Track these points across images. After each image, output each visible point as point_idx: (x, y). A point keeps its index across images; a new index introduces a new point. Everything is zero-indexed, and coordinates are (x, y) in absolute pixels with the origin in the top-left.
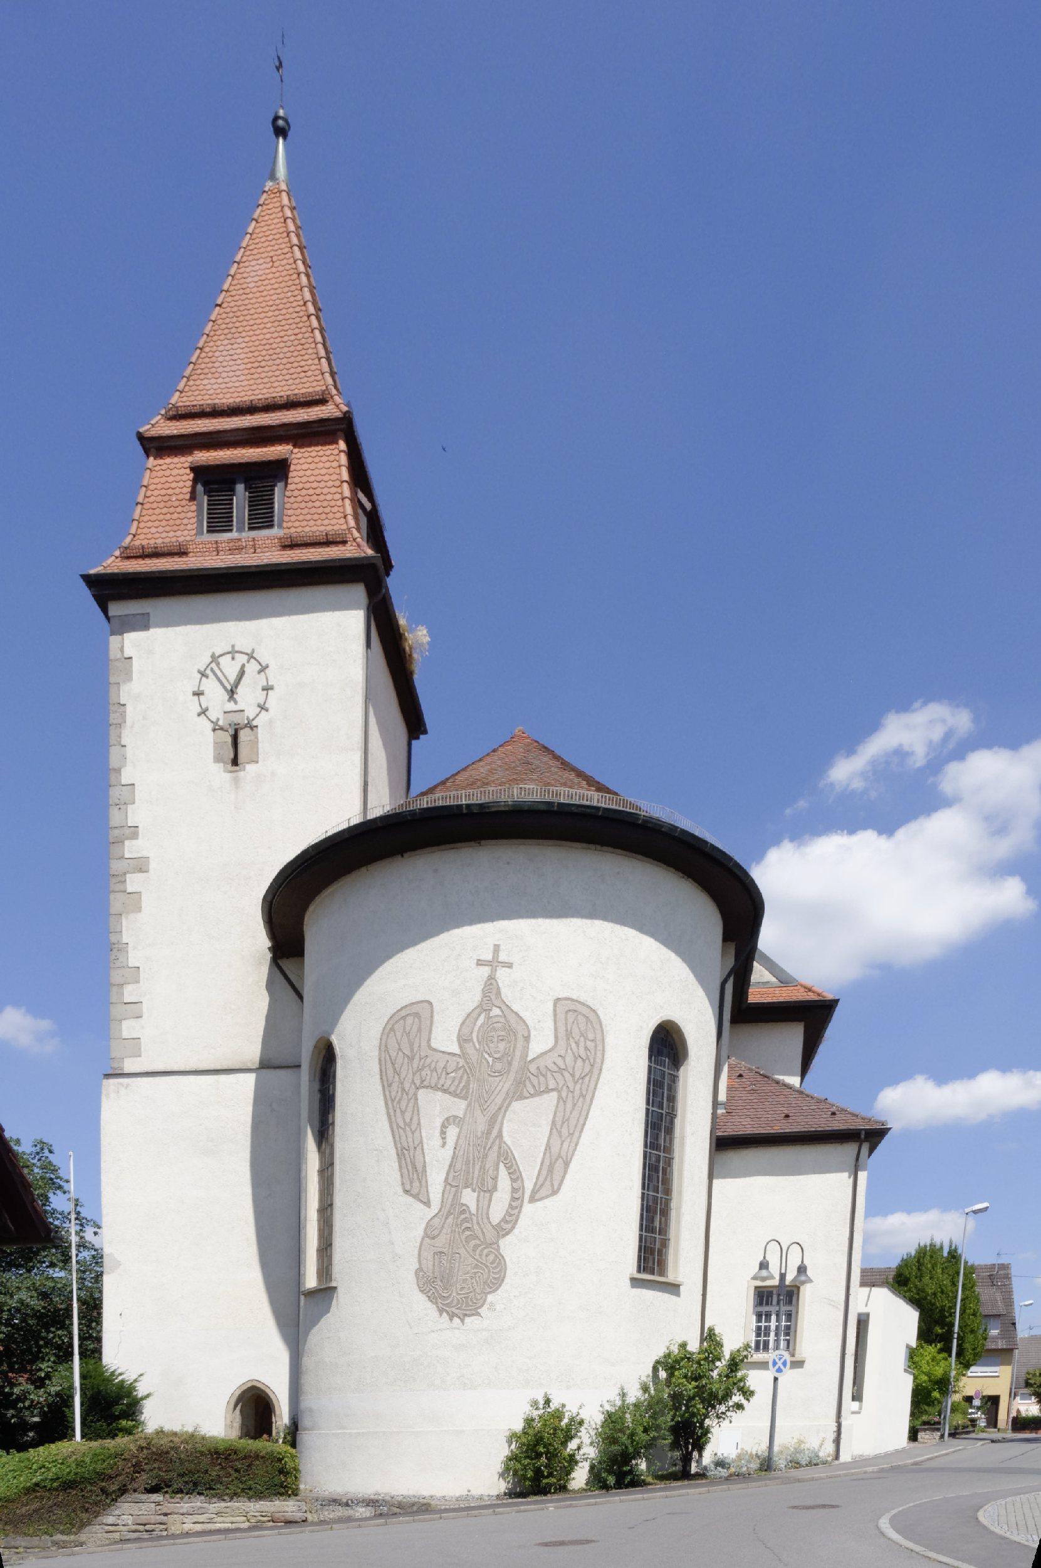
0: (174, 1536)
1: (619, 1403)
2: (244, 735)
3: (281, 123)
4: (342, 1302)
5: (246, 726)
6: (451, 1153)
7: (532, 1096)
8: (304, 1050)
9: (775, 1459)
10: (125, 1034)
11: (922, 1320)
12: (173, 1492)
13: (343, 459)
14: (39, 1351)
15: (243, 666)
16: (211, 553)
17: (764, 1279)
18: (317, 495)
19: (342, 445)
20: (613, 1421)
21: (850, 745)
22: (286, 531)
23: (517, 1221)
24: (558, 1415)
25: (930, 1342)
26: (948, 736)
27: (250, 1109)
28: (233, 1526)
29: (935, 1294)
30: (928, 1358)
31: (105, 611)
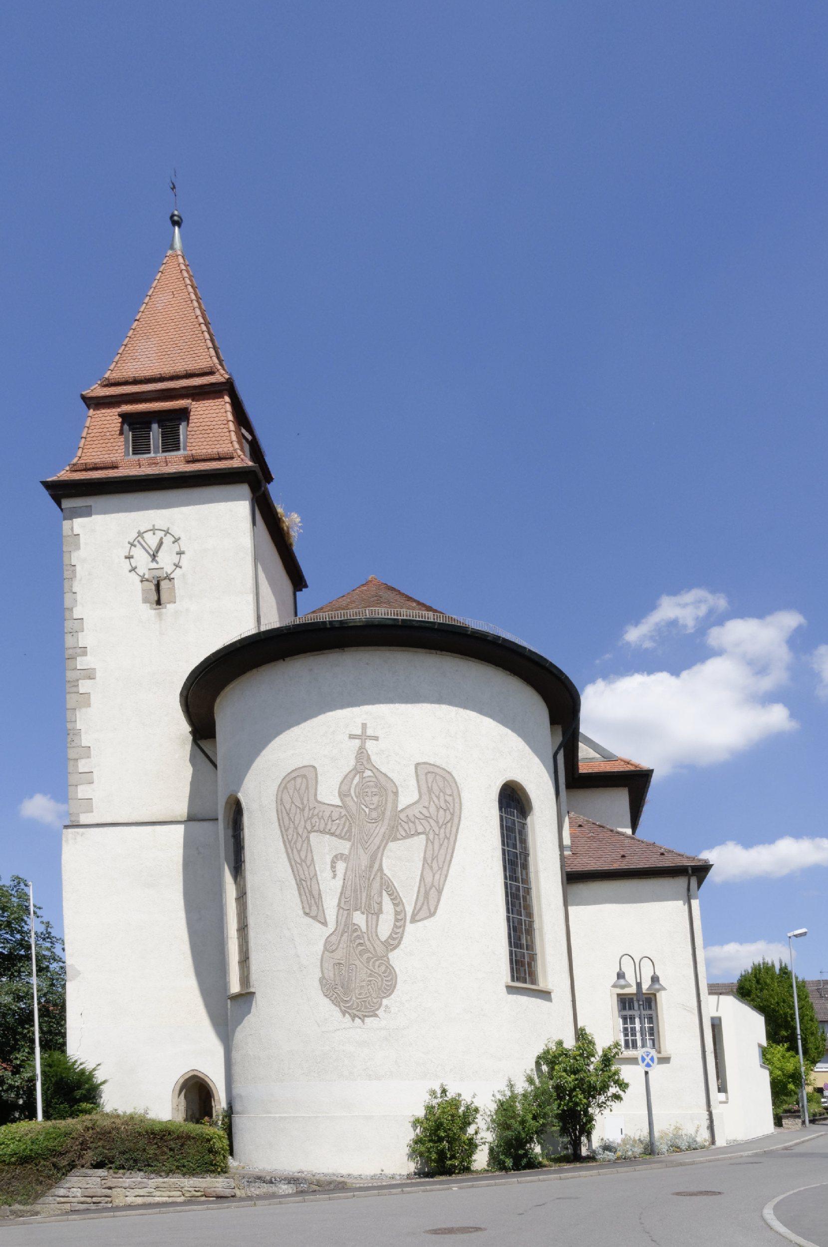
0: (117, 1208)
1: (509, 1094)
2: (164, 585)
3: (176, 218)
4: (260, 1003)
5: (165, 578)
6: (341, 883)
7: (404, 838)
8: (219, 806)
9: (658, 1144)
10: (80, 796)
11: (768, 1022)
12: (116, 1168)
13: (228, 407)
14: (16, 1044)
15: (161, 539)
16: (133, 466)
17: (623, 987)
18: (210, 430)
19: (227, 399)
20: (505, 1109)
21: (637, 616)
22: (190, 453)
23: (402, 937)
24: (455, 1103)
25: (778, 1042)
26: (711, 612)
27: (181, 851)
28: (171, 1200)
29: (778, 1003)
30: (779, 1056)
31: (59, 504)
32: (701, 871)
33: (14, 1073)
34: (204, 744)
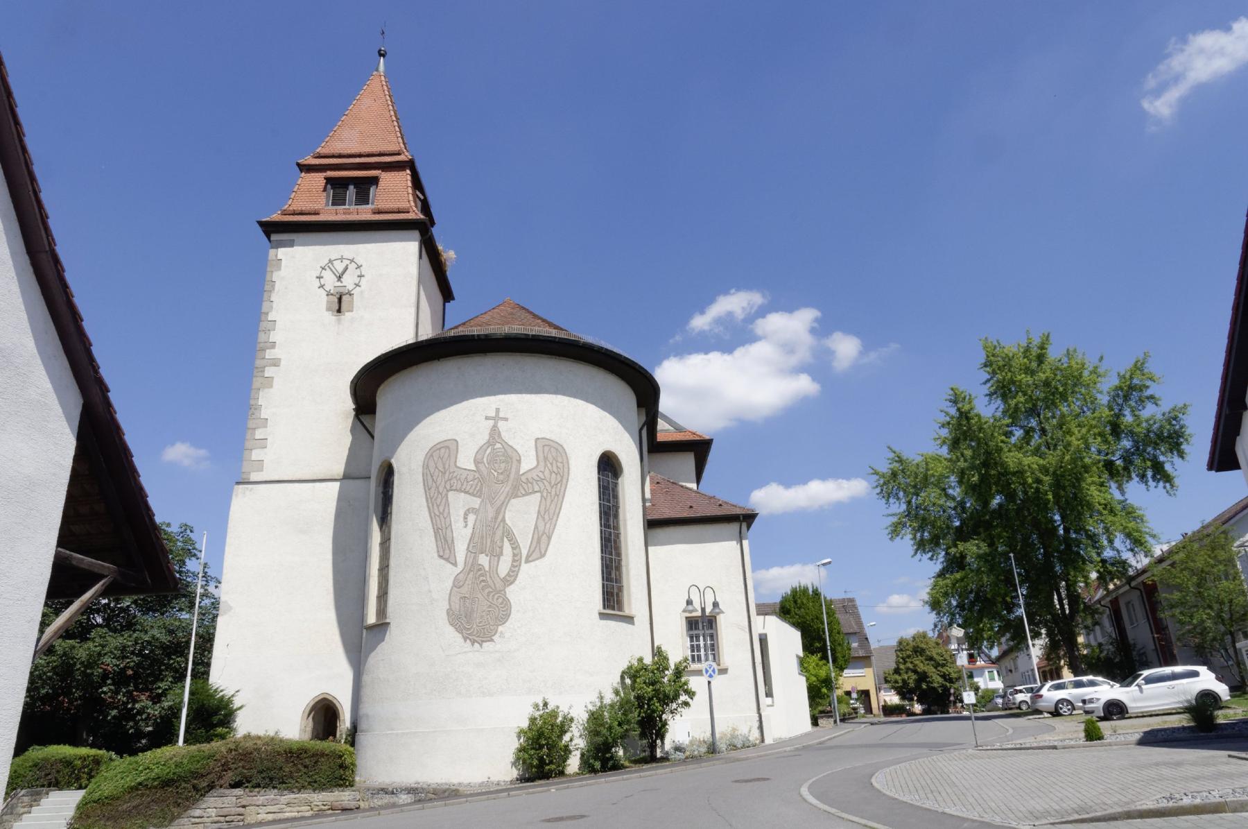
2: (344, 298)
10: (253, 458)
13: (409, 178)
16: (332, 214)
17: (691, 612)
18: (394, 192)
31: (269, 238)
32: (747, 518)
33: (155, 703)
34: (364, 418)
